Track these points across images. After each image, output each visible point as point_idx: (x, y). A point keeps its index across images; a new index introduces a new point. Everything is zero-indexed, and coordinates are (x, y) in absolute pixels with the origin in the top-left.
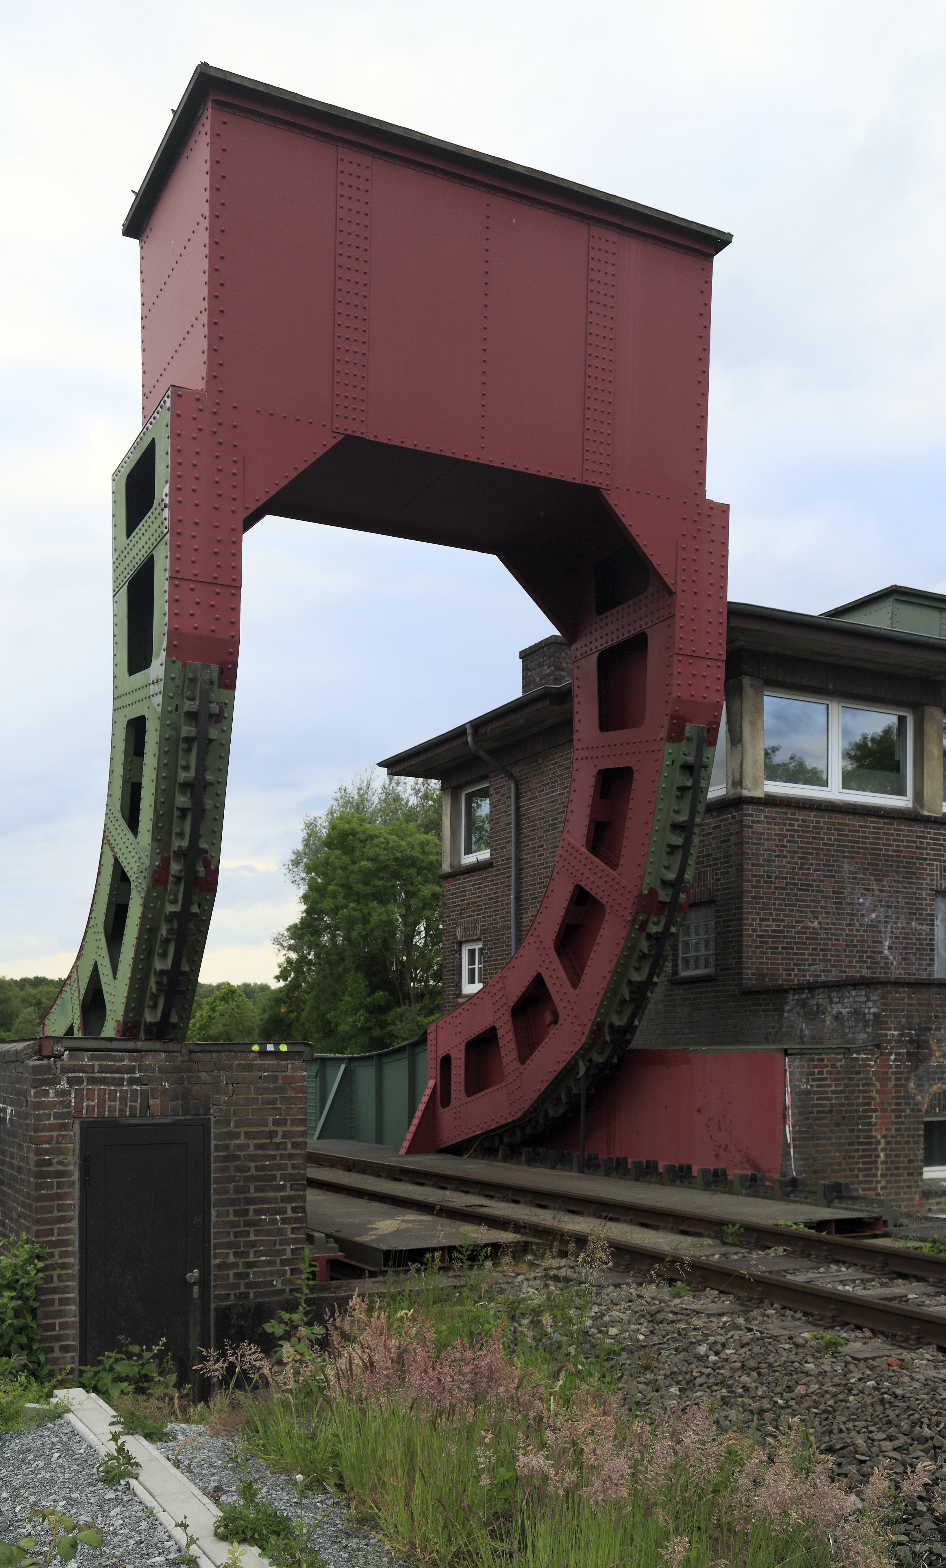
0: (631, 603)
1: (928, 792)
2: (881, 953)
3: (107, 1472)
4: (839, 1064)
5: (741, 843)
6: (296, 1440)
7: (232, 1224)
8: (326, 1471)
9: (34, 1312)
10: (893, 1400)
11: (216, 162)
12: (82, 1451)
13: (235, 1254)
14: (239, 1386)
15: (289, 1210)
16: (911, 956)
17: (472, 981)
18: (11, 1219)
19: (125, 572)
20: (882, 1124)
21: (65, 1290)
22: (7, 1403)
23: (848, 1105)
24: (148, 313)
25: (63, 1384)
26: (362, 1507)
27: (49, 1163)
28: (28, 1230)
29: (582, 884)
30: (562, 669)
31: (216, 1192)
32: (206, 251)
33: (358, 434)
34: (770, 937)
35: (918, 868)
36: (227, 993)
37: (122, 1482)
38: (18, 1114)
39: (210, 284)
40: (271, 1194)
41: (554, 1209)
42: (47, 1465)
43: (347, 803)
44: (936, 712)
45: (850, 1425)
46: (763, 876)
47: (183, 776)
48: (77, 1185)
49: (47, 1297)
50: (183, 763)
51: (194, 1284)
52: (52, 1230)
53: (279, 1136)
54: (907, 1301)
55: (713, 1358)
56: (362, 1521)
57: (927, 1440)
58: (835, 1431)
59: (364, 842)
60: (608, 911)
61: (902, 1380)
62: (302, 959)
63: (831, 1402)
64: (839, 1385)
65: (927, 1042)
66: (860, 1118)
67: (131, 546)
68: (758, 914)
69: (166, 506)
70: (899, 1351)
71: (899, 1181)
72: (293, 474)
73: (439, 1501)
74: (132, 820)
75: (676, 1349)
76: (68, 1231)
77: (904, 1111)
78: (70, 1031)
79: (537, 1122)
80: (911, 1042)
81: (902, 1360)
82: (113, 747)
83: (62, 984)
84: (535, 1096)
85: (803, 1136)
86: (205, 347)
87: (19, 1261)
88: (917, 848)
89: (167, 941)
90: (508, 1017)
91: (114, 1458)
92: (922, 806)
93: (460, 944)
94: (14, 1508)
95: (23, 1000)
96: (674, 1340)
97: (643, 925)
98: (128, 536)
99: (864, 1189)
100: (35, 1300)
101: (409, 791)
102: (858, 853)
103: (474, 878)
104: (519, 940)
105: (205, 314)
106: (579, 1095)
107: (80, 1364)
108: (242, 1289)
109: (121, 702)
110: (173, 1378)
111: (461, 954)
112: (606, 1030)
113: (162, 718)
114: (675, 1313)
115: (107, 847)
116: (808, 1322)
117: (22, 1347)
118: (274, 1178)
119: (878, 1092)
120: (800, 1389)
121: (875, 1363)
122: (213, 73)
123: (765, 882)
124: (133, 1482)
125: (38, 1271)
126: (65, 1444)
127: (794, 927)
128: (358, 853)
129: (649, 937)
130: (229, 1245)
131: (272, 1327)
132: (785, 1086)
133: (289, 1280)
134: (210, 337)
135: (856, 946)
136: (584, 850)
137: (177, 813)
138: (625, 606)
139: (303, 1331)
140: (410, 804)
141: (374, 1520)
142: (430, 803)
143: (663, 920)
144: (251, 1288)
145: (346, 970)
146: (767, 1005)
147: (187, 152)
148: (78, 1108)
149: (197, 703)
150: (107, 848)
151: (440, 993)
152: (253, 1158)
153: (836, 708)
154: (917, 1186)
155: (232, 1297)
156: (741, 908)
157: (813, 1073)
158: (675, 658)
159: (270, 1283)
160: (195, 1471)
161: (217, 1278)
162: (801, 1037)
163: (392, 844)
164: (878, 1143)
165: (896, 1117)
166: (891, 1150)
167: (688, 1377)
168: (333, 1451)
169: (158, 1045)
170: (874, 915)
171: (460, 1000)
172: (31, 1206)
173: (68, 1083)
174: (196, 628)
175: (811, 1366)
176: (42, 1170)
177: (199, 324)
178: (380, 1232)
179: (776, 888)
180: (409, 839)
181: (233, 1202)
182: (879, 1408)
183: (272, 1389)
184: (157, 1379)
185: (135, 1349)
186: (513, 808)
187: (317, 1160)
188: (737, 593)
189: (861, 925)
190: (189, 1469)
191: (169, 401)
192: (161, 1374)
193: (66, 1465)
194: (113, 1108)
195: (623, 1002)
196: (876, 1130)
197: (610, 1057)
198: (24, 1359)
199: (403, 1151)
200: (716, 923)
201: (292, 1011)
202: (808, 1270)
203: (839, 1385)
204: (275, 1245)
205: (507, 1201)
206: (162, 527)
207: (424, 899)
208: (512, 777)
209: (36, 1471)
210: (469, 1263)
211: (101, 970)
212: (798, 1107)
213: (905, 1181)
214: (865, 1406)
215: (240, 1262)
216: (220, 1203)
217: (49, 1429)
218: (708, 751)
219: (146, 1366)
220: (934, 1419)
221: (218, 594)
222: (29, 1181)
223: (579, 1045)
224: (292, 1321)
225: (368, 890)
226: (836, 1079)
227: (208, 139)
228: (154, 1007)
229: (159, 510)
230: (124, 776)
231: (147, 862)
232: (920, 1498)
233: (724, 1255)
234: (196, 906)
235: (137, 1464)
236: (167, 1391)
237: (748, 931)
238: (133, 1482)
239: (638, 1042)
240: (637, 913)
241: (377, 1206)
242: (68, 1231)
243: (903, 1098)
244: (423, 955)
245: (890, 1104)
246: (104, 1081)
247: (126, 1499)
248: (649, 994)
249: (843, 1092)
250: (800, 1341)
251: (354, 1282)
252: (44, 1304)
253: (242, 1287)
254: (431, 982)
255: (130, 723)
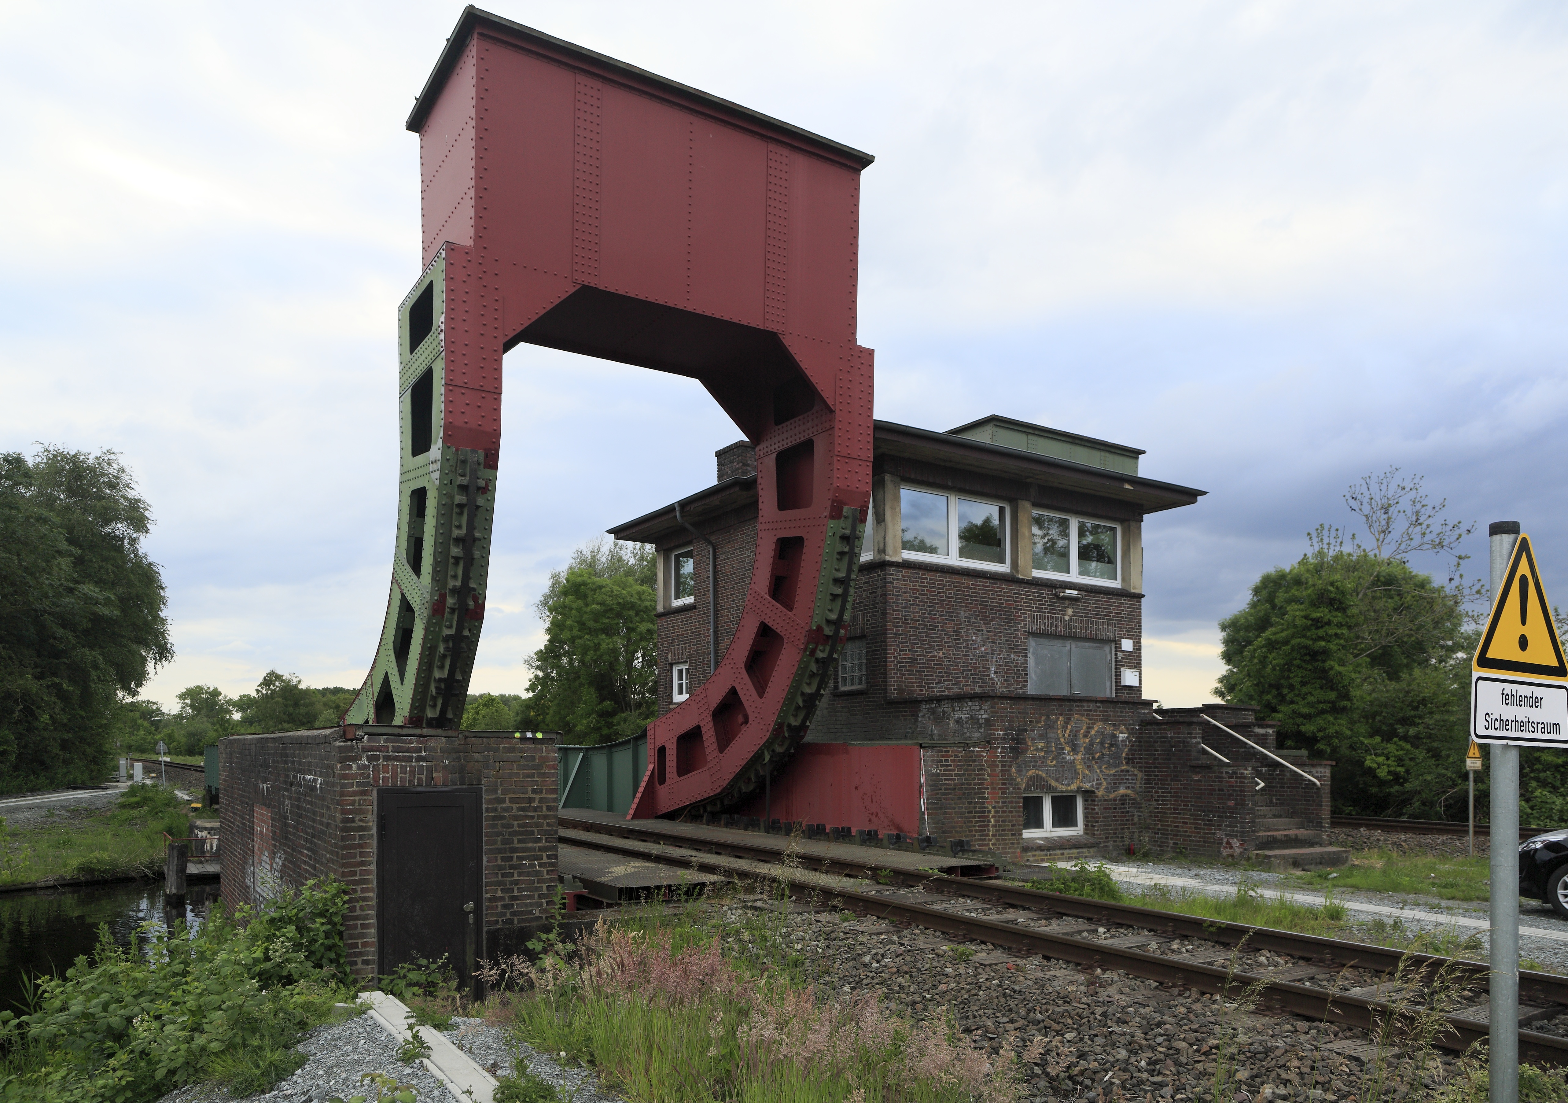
0: (801, 417)
1: (1021, 561)
2: (989, 676)
3: (405, 1054)
4: (960, 755)
5: (885, 594)
6: (556, 1028)
7: (500, 868)
8: (580, 1051)
9: (341, 934)
10: (1012, 993)
11: (480, 79)
12: (383, 1038)
13: (502, 890)
14: (509, 987)
15: (545, 857)
16: (1010, 679)
17: (681, 692)
18: (321, 864)
19: (409, 380)
20: (992, 798)
21: (366, 917)
22: (320, 1003)
23: (968, 784)
24: (426, 188)
25: (365, 989)
26: (610, 1078)
27: (352, 820)
28: (335, 871)
29: (766, 622)
30: (748, 465)
31: (487, 843)
32: (473, 143)
33: (592, 285)
34: (907, 663)
35: (1015, 616)
36: (489, 701)
37: (417, 1061)
38: (326, 783)
39: (476, 168)
40: (530, 845)
41: (748, 858)
42: (355, 1049)
43: (583, 561)
44: (1027, 505)
45: (981, 1012)
46: (901, 619)
47: (456, 533)
48: (375, 837)
49: (352, 922)
50: (457, 523)
51: (470, 912)
52: (355, 871)
53: (537, 802)
54: (1017, 924)
55: (875, 965)
56: (610, 1087)
57: (1039, 1022)
58: (970, 1017)
59: (594, 590)
60: (785, 641)
61: (1019, 979)
62: (547, 676)
63: (966, 996)
64: (971, 983)
65: (1025, 739)
66: (976, 793)
67: (414, 360)
68: (898, 646)
69: (442, 331)
70: (1015, 959)
71: (1005, 840)
72: (542, 312)
73: (675, 1068)
74: (416, 565)
75: (846, 959)
76: (368, 872)
77: (1008, 789)
78: (367, 721)
79: (733, 796)
80: (1013, 739)
81: (1018, 965)
82: (400, 510)
83: (356, 693)
84: (731, 777)
85: (935, 806)
86: (473, 214)
87: (328, 896)
88: (1014, 601)
89: (444, 657)
90: (710, 718)
91: (410, 1043)
92: (1017, 572)
93: (671, 665)
94: (329, 1082)
95: (325, 705)
96: (845, 952)
97: (813, 652)
98: (411, 353)
99: (979, 845)
100: (341, 925)
101: (629, 555)
102: (971, 604)
103: (682, 617)
104: (717, 663)
105: (473, 190)
106: (765, 776)
107: (379, 974)
108: (508, 916)
109: (405, 477)
110: (454, 984)
111: (672, 673)
112: (785, 729)
113: (439, 489)
114: (846, 933)
115: (395, 586)
116: (944, 939)
117: (331, 961)
118: (533, 833)
119: (988, 775)
120: (943, 987)
121: (998, 967)
122: (478, 13)
123: (903, 623)
124: (426, 1061)
125: (344, 903)
126: (369, 1033)
127: (925, 656)
128: (590, 599)
129: (817, 661)
130: (498, 884)
131: (533, 944)
132: (921, 770)
133: (545, 910)
134: (476, 207)
135: (970, 671)
136: (767, 596)
137: (451, 561)
138: (797, 419)
139: (559, 946)
140: (630, 563)
141: (619, 1087)
142: (645, 563)
143: (828, 648)
144: (516, 916)
145: (581, 685)
146: (906, 712)
147: (458, 70)
148: (376, 779)
149: (468, 478)
150: (395, 586)
151: (653, 703)
152: (516, 818)
153: (954, 499)
154: (1018, 843)
155: (500, 923)
156: (885, 641)
157: (941, 761)
158: (835, 458)
159: (531, 912)
160: (476, 1052)
161: (488, 908)
162: (932, 735)
163: (615, 592)
164: (990, 812)
165: (1002, 793)
166: (999, 817)
167: (857, 979)
168: (585, 1036)
169: (439, 732)
170: (983, 649)
171: (672, 707)
172: (338, 853)
173: (367, 759)
174: (466, 423)
175: (950, 970)
176: (347, 826)
177: (467, 197)
178: (615, 875)
179: (911, 628)
180: (629, 589)
181: (500, 851)
182: (1003, 1000)
183: (537, 990)
184: (441, 984)
185: (424, 962)
186: (711, 566)
187: (564, 823)
188: (881, 413)
189: (974, 656)
190: (470, 1051)
191: (444, 253)
192: (445, 981)
193: (371, 1049)
194: (403, 779)
195: (798, 708)
196: (988, 803)
197: (789, 748)
198: (333, 969)
199: (629, 817)
200: (867, 652)
201: (539, 715)
202: (942, 902)
203: (971, 983)
204: (534, 883)
205: (712, 853)
206: (439, 347)
207: (641, 633)
208: (710, 543)
209: (347, 1054)
210: (685, 897)
211: (391, 678)
212: (930, 786)
213: (1009, 839)
214: (992, 998)
215: (507, 896)
216: (490, 851)
217: (355, 1022)
218: (860, 527)
219: (433, 975)
220: (1044, 1007)
221: (483, 398)
222: (336, 834)
223: (765, 739)
224: (549, 940)
225: (598, 626)
226: (958, 766)
227: (474, 61)
228: (434, 706)
229: (436, 333)
230: (409, 532)
231: (428, 597)
232: (1036, 1064)
233: (879, 891)
234: (467, 630)
235: (428, 1047)
236: (450, 994)
237: (891, 658)
238: (426, 1061)
239: (809, 737)
240: (808, 643)
241: (611, 856)
242: (368, 872)
243: (1007, 779)
244: (640, 675)
245: (998, 784)
246: (396, 758)
247: (420, 1074)
248: (817, 702)
249: (963, 775)
250: (941, 952)
251: (595, 912)
252: (349, 928)
253: (508, 915)
254: (647, 695)
255: (413, 492)
